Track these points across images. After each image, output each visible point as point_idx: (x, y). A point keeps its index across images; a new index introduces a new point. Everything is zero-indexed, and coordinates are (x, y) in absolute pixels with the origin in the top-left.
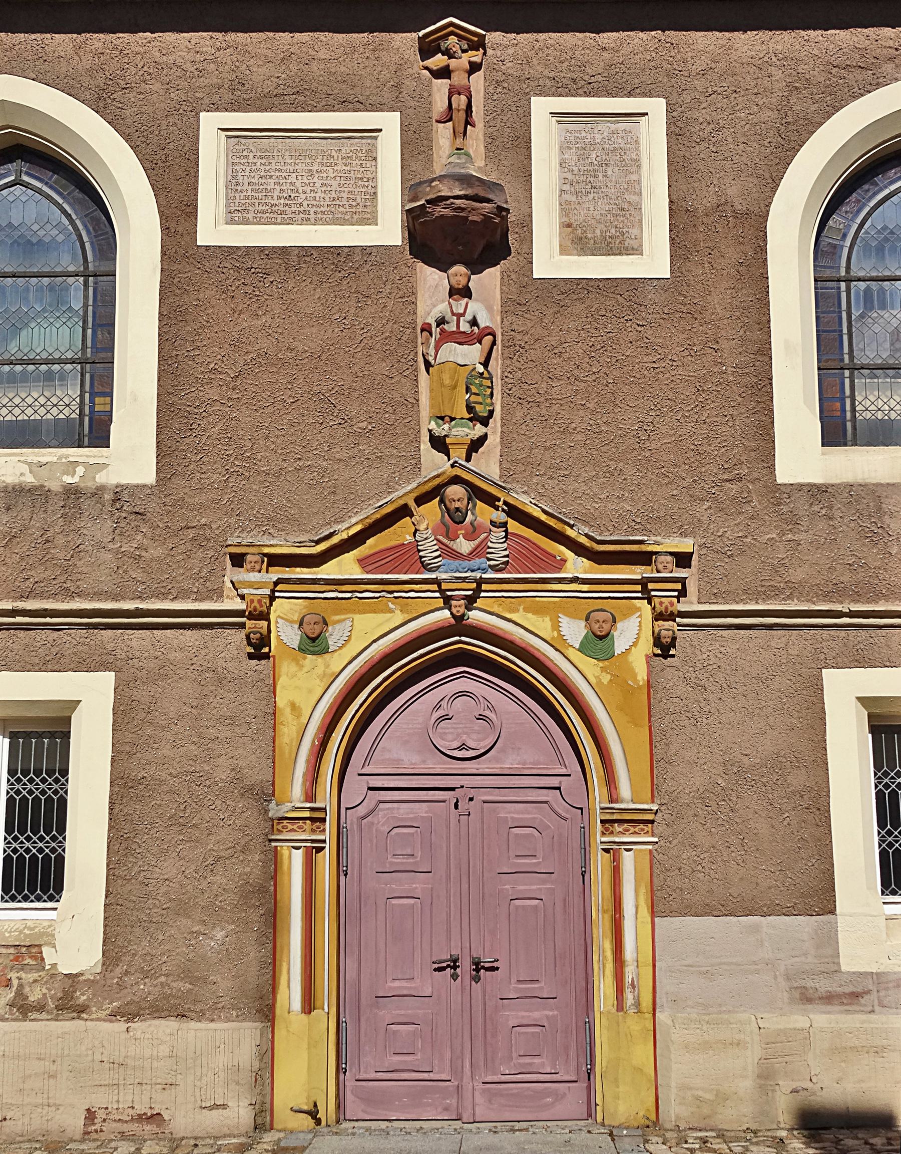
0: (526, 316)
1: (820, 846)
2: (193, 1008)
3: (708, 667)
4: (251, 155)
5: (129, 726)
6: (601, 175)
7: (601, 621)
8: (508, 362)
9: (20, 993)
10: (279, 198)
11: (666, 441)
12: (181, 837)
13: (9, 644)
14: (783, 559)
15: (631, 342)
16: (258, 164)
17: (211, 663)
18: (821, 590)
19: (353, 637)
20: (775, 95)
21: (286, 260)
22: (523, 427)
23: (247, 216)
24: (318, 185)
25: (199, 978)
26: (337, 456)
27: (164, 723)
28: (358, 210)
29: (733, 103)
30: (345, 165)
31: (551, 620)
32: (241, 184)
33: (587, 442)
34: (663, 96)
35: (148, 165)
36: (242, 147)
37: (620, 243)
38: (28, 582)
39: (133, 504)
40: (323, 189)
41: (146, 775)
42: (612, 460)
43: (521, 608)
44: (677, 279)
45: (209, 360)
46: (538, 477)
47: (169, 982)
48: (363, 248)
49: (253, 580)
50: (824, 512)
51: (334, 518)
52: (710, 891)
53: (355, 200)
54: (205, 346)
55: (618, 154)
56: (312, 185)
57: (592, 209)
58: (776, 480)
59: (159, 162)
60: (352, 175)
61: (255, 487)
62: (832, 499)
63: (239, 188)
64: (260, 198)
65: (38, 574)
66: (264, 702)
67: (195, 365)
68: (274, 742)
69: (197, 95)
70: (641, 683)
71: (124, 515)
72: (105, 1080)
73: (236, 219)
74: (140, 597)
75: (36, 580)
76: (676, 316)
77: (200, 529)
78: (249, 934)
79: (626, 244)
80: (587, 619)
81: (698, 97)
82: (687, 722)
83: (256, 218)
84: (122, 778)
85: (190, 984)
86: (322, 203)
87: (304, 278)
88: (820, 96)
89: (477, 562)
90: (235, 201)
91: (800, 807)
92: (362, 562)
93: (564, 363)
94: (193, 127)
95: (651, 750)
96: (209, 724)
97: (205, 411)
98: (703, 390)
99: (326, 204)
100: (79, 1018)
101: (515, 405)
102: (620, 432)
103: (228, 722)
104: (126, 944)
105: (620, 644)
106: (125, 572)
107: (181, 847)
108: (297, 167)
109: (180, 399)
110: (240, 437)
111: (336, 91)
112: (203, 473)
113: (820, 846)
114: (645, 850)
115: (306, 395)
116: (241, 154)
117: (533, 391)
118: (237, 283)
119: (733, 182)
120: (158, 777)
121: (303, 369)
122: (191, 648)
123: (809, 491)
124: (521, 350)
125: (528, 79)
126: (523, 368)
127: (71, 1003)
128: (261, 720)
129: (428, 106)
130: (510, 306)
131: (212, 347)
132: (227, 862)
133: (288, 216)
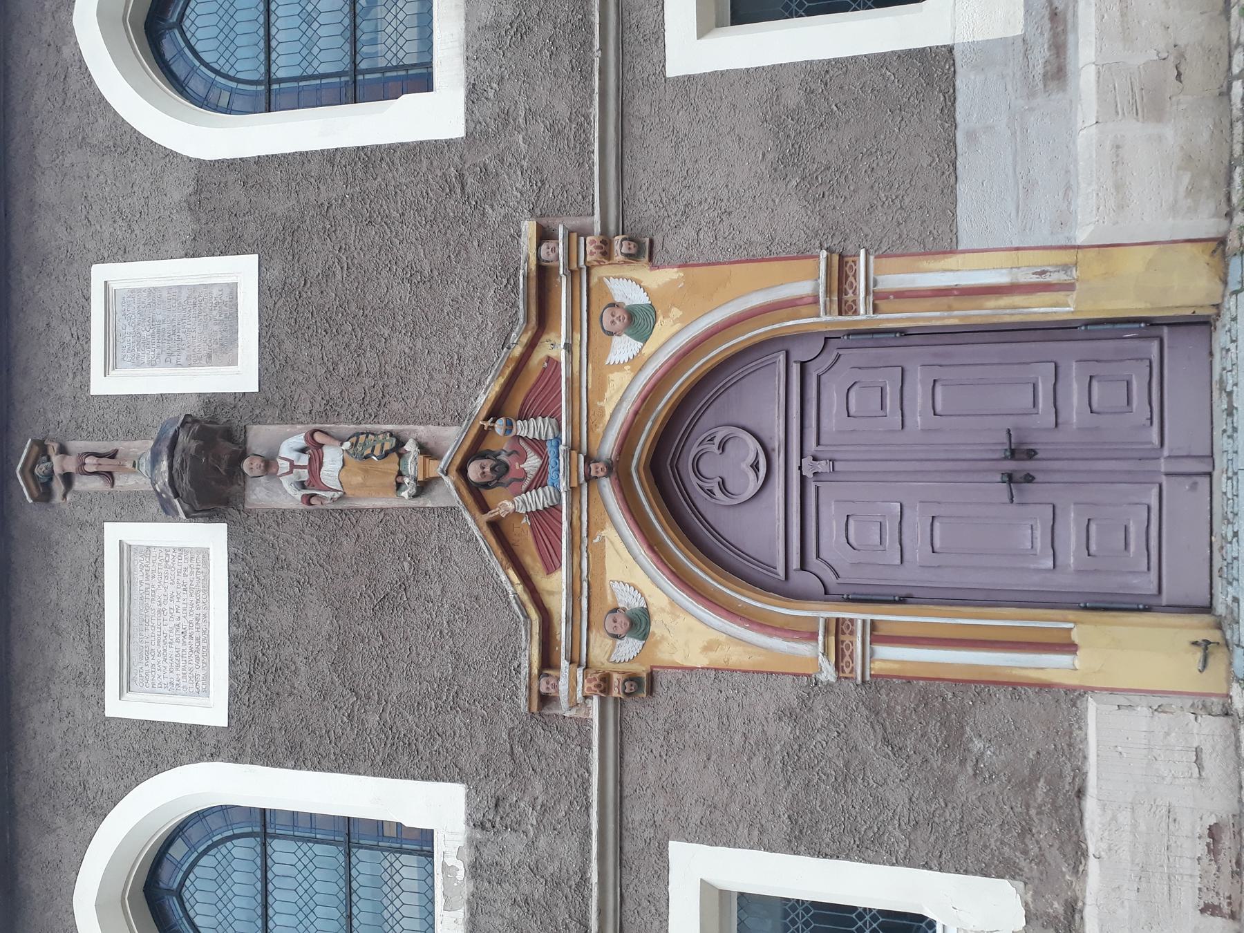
0: (296, 399)
2: (1069, 779)
4: (145, 668)
5: (730, 829)
6: (162, 326)
8: (343, 417)
12: (860, 781)
15: (322, 292)
16: (153, 662)
18: (579, 83)
27: (727, 792)
30: (153, 577)
31: (612, 372)
38: (571, 926)
39: (487, 809)
41: (786, 816)
48: (231, 561)
50: (495, 86)
53: (186, 569)
56: (172, 611)
57: (194, 334)
58: (462, 138)
63: (175, 682)
70: (682, 274)
71: (498, 819)
72: (1163, 889)
75: (567, 916)
80: (611, 334)
82: (726, 223)
84: (790, 841)
85: (1038, 780)
86: (189, 602)
89: (550, 450)
90: (188, 687)
91: (825, 92)
92: (551, 567)
98: (370, 217)
100: (1081, 911)
102: (414, 302)
105: (640, 298)
107: (871, 782)
109: (378, 754)
111: (86, 584)
117: (372, 391)
118: (264, 689)
123: (473, 102)
127: (1062, 919)
128: (724, 685)
130: (286, 414)
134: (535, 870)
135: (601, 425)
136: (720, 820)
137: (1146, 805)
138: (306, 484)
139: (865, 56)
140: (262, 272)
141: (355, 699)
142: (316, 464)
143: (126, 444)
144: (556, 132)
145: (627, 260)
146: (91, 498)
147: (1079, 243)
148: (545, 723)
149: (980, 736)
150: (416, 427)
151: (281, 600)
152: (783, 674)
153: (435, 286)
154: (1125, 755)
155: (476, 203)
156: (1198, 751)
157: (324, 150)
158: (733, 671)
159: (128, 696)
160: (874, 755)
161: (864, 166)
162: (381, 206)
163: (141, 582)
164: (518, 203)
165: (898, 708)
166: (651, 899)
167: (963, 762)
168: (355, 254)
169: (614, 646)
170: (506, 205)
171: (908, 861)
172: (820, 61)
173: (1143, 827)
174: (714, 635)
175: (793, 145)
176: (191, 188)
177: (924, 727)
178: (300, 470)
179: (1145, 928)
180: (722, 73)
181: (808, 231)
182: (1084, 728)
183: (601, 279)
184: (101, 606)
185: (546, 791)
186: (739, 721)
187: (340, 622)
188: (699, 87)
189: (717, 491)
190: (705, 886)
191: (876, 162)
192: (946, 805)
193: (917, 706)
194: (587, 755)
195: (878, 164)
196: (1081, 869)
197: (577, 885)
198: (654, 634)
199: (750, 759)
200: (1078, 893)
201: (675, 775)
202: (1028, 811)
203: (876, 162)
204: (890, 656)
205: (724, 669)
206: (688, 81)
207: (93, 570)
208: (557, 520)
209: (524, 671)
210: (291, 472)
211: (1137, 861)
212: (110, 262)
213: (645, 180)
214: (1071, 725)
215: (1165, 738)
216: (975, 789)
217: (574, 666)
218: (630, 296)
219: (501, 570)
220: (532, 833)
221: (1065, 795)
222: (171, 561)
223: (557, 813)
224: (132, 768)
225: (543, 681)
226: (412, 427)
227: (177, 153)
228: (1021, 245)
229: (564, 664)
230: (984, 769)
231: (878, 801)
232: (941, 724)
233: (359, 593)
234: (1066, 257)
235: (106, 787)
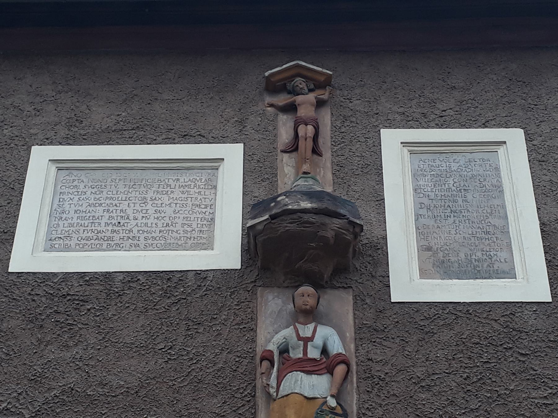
0: (385, 343)
4: (82, 186)
8: (366, 397)
15: (514, 374)
16: (89, 193)
28: (193, 236)
30: (183, 193)
34: (520, 127)
37: (488, 266)
48: (197, 273)
56: (144, 211)
57: (453, 232)
63: (64, 216)
69: (32, 131)
73: (57, 246)
108: (130, 195)
118: (49, 311)
124: (381, 382)
125: (377, 114)
138: (285, 355)
143: (329, 165)
222: (200, 210)
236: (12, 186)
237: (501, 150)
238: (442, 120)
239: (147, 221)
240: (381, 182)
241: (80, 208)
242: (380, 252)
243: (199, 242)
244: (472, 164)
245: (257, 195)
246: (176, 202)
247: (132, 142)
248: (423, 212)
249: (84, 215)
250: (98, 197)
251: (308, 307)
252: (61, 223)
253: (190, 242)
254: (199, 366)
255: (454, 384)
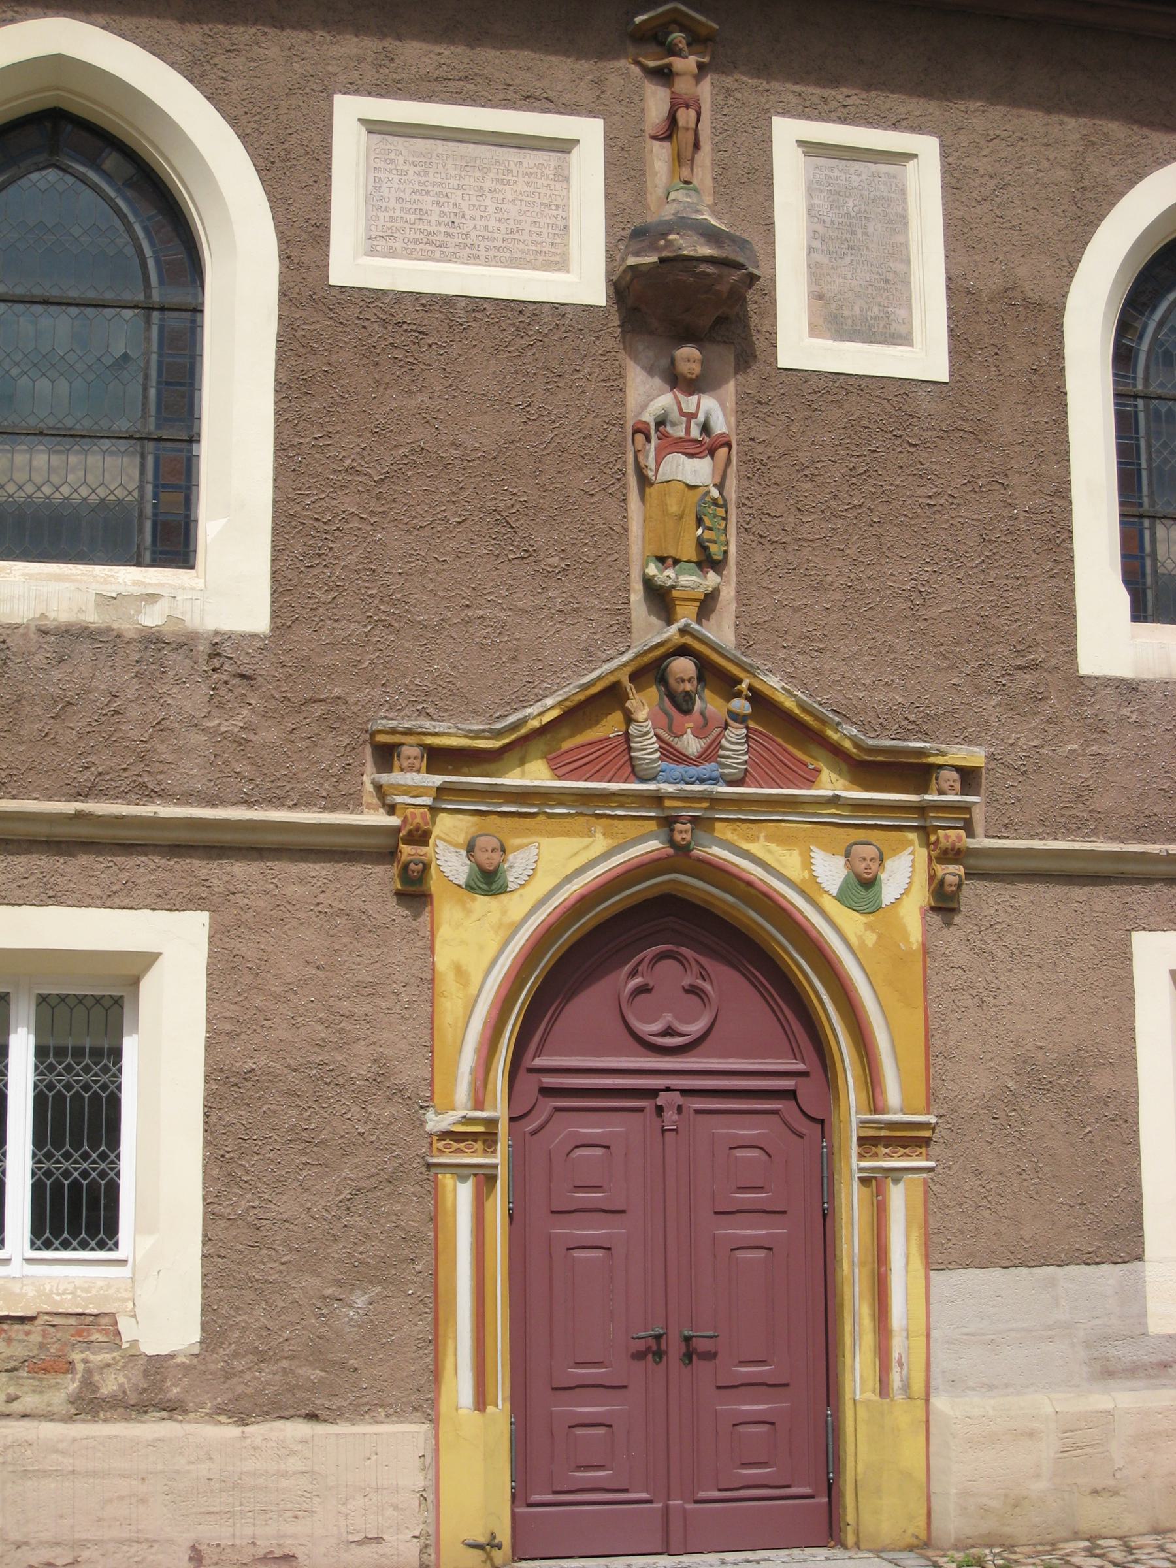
0: (768, 420)
1: (1126, 1169)
2: (327, 1404)
3: (996, 926)
4: (401, 160)
5: (230, 993)
6: (859, 231)
7: (868, 859)
8: (746, 483)
9: (88, 1383)
10: (439, 223)
11: (944, 608)
12: (304, 1159)
13: (59, 864)
14: (1087, 780)
15: (901, 467)
16: (411, 173)
17: (344, 902)
18: (1132, 824)
19: (539, 873)
20: (1069, 149)
21: (450, 315)
22: (765, 576)
23: (394, 245)
24: (491, 209)
25: (334, 1363)
26: (520, 604)
27: (279, 990)
28: (543, 249)
29: (1019, 155)
30: (527, 184)
31: (801, 854)
32: (387, 200)
33: (848, 604)
34: (935, 134)
35: (261, 164)
36: (389, 147)
37: (885, 326)
38: (87, 774)
39: (239, 663)
40: (498, 216)
41: (254, 1066)
42: (878, 631)
43: (762, 835)
44: (957, 385)
45: (344, 454)
46: (785, 651)
47: (293, 1368)
48: (555, 306)
49: (410, 783)
50: (1134, 717)
51: (516, 695)
52: (998, 1234)
53: (539, 235)
54: (338, 432)
55: (880, 206)
56: (483, 209)
57: (849, 277)
58: (1078, 671)
59: (277, 160)
60: (536, 199)
61: (407, 645)
62: (1144, 700)
63: (383, 204)
64: (412, 221)
65: (103, 760)
66: (419, 964)
67: (325, 460)
68: (432, 1022)
69: (329, 68)
70: (914, 947)
71: (225, 677)
72: (215, 1506)
73: (379, 248)
74: (246, 802)
75: (100, 769)
76: (957, 435)
77: (330, 703)
78: (401, 1300)
79: (893, 330)
80: (847, 855)
81: (977, 140)
82: (970, 1003)
83: (406, 249)
84: (222, 1070)
85: (323, 1370)
86: (496, 235)
87: (474, 343)
88: (1121, 157)
89: (706, 769)
90: (377, 223)
91: (1105, 1118)
93: (817, 489)
94: (323, 113)
95: (927, 1041)
96: (343, 992)
97: (338, 529)
98: (990, 541)
99: (501, 237)
100: (171, 1418)
101: (754, 545)
102: (888, 592)
103: (369, 990)
104: (233, 1313)
105: (889, 890)
106: (226, 763)
107: (304, 1173)
108: (463, 182)
109: (304, 509)
110: (386, 570)
111: (517, 81)
112: (336, 621)
113: (1126, 1169)
114: (918, 1179)
115: (476, 513)
116: (387, 157)
117: (778, 527)
118: (383, 343)
119: (1022, 259)
120: (272, 1070)
121: (473, 475)
122: (314, 880)
123: (1117, 688)
124: (762, 467)
125: (768, 91)
126: (765, 492)
127: (160, 1397)
128: (413, 989)
129: (639, 114)
130: (747, 407)
131: (348, 434)
132: (370, 1195)
133: (449, 250)
134: (160, 727)
135: (735, 838)
136: (241, 980)
137: (311, 1486)
138: (661, 428)
139: (1140, 1164)
140: (927, 385)
141: (376, 479)
142: (693, 449)
143: (708, 162)
144: (1082, 793)
145: (936, 882)
146: (635, 103)
147: (933, 1400)
148: (354, 749)
149: (371, 1304)
150: (733, 585)
151: (505, 378)
152: (432, 1066)
153: (907, 623)
154: (368, 1462)
155: (1004, 685)
156: (378, 1540)
157: (1070, 484)
158: (432, 1002)
159: (363, 130)
160: (339, 1176)
161: (1025, 1164)
162: (1002, 557)
163: (521, 163)
164: (1002, 740)
165: (398, 1207)
166: (129, 887)
167: (339, 1283)
168: (946, 517)
169: (456, 845)
170: (1001, 725)
171: (211, 1216)
172: (1137, 1113)
173: (284, 1483)
174: (476, 978)
175: (1050, 1082)
176: (1030, 294)
177: (377, 1238)
178: (684, 426)
179: (166, 1488)
180: (1132, 999)
181: (957, 1100)
182: (388, 1420)
183: (911, 843)
184: (487, 103)
185: (264, 746)
186: (368, 1009)
187: (477, 462)
188: (1119, 971)
189: (638, 981)
190: (149, 959)
191: (1028, 1177)
192: (283, 1264)
193: (403, 1229)
194: (315, 805)
195: (1025, 1180)
196: (221, 1418)
197: (144, 785)
198: (474, 900)
199: (321, 1021)
200: (192, 1415)
201: (295, 923)
202: (286, 1358)
203: (1028, 1177)
204: (463, 1195)
205: (433, 991)
206: (1125, 956)
207: (538, 93)
208: (612, 778)
209: (428, 725)
210: (682, 414)
211: (244, 1477)
212: (943, 166)
213: (1022, 904)
214: (391, 1406)
215: (392, 1505)
216: (306, 1297)
217: (434, 794)
218: (891, 880)
219: (560, 699)
220: (210, 724)
221: (309, 1400)
222: (550, 212)
223: (237, 761)
224: (262, 130)
225: (416, 751)
226: (734, 579)
227: (1073, 277)
228: (932, 1340)
229: (438, 780)
230: (331, 1308)
231: (283, 1180)
232: (383, 1258)
233: (516, 491)
234: (918, 1386)
235: (233, 86)
236: (315, 155)
237: (911, 165)
238: (845, 111)
239: (487, 223)
240: (770, 197)
241: (402, 195)
242: (767, 298)
243: (551, 259)
244: (876, 179)
245: (621, 200)
246: (520, 198)
247: (461, 101)
248: (817, 244)
249: (408, 206)
250: (423, 179)
251: (694, 376)
252: (381, 215)
253: (541, 258)
254: (562, 430)
255: (839, 475)
